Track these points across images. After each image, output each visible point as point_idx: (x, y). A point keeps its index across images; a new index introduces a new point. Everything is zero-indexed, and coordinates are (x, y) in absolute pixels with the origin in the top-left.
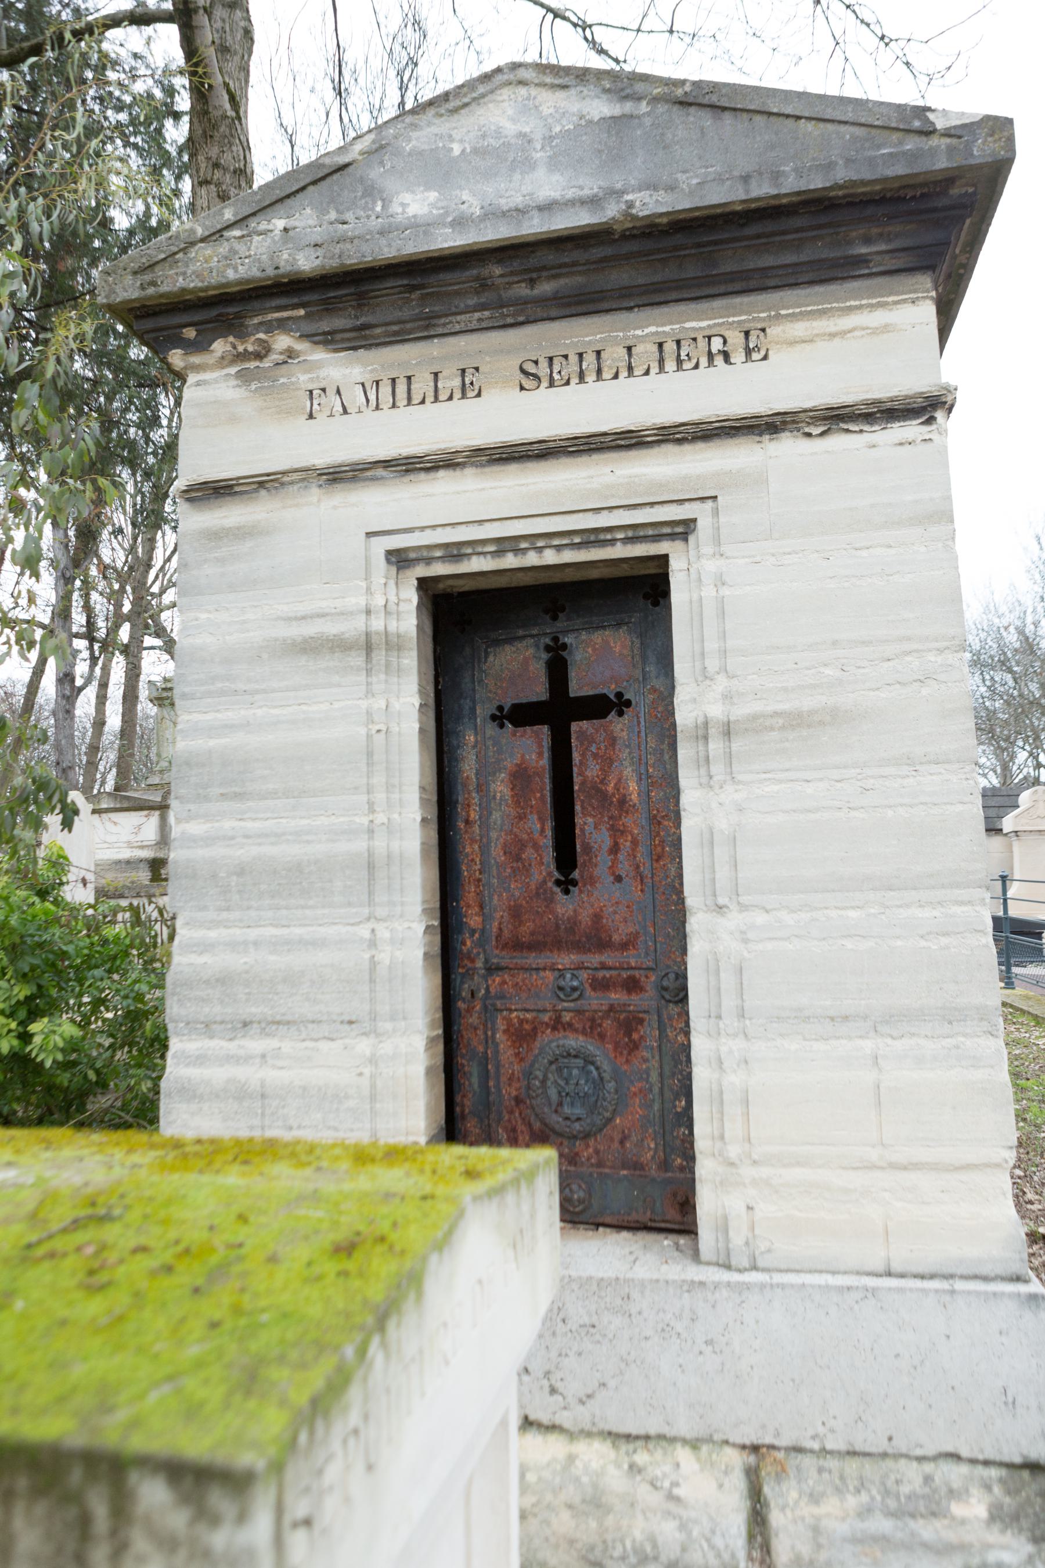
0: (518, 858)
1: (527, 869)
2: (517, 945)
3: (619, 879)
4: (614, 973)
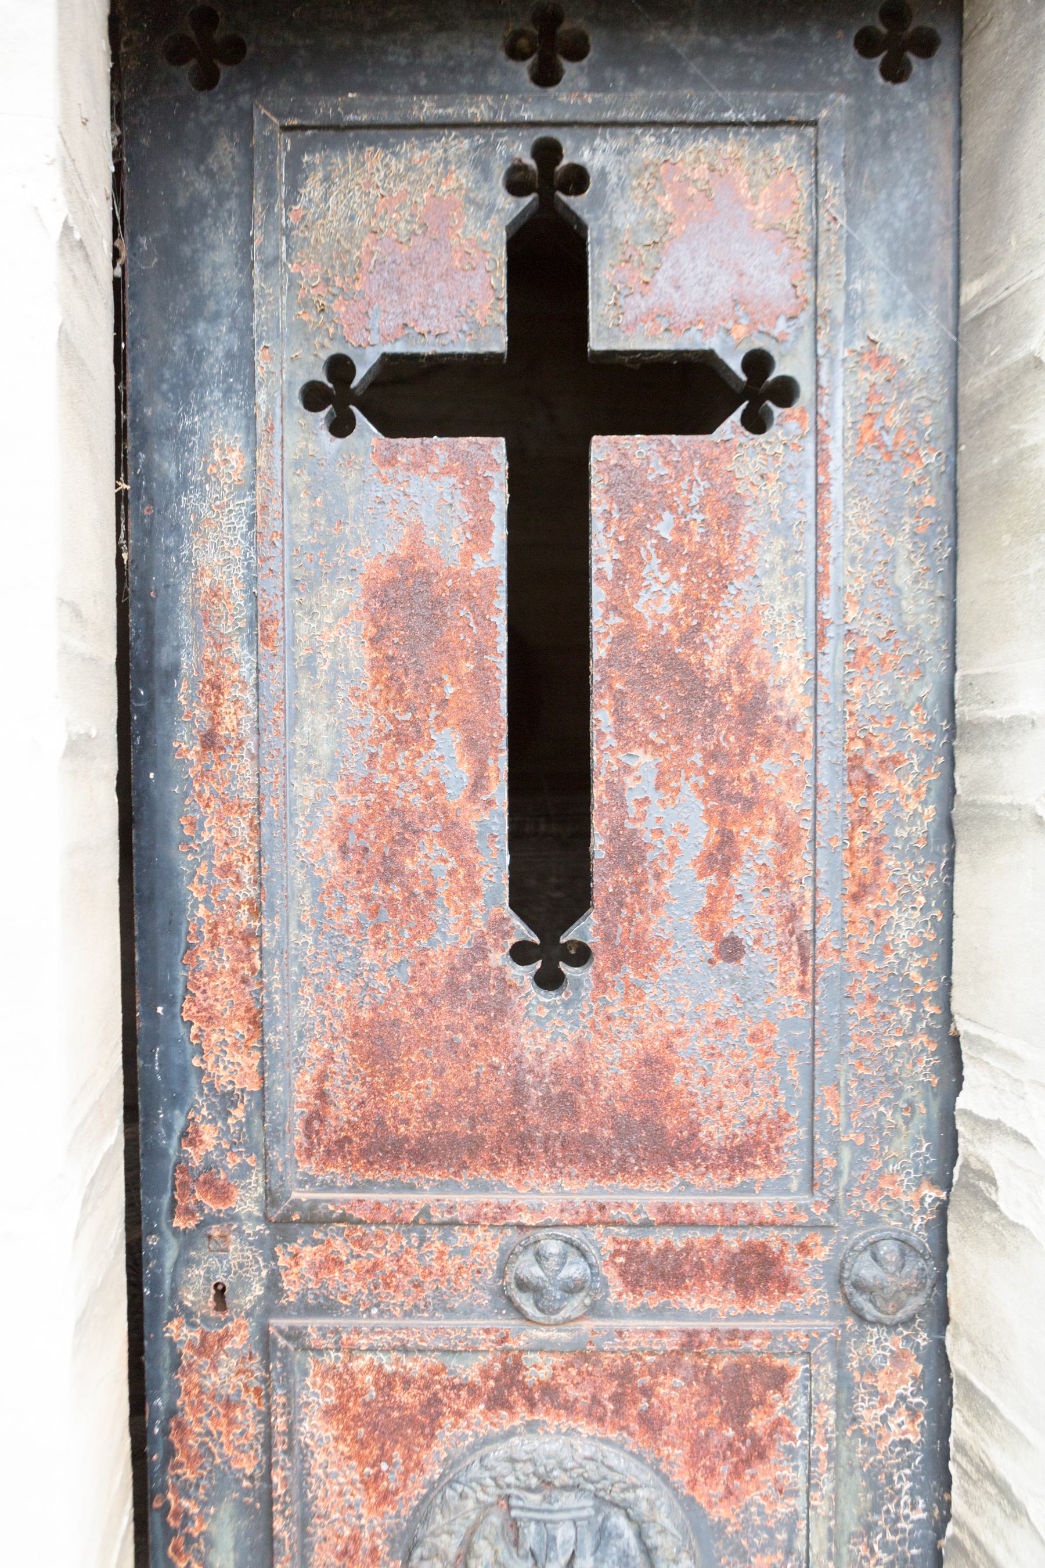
0: (390, 872)
1: (418, 905)
2: (381, 1148)
3: (731, 949)
4: (700, 1237)
